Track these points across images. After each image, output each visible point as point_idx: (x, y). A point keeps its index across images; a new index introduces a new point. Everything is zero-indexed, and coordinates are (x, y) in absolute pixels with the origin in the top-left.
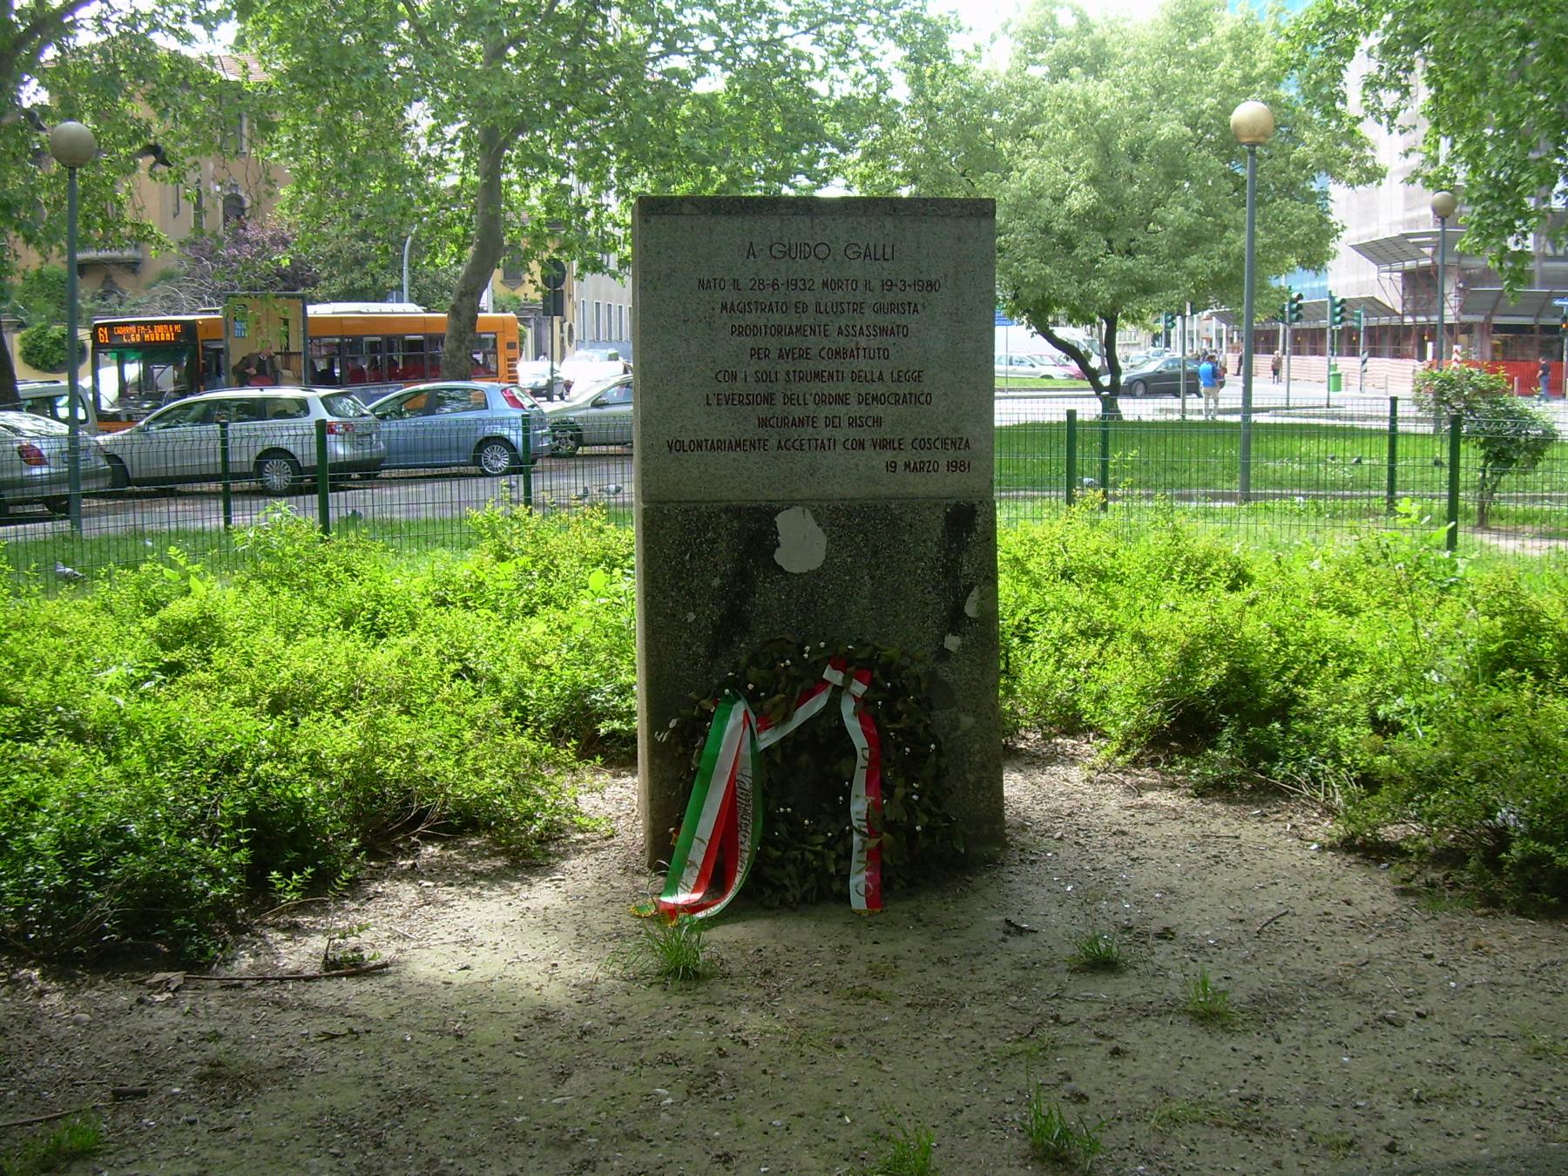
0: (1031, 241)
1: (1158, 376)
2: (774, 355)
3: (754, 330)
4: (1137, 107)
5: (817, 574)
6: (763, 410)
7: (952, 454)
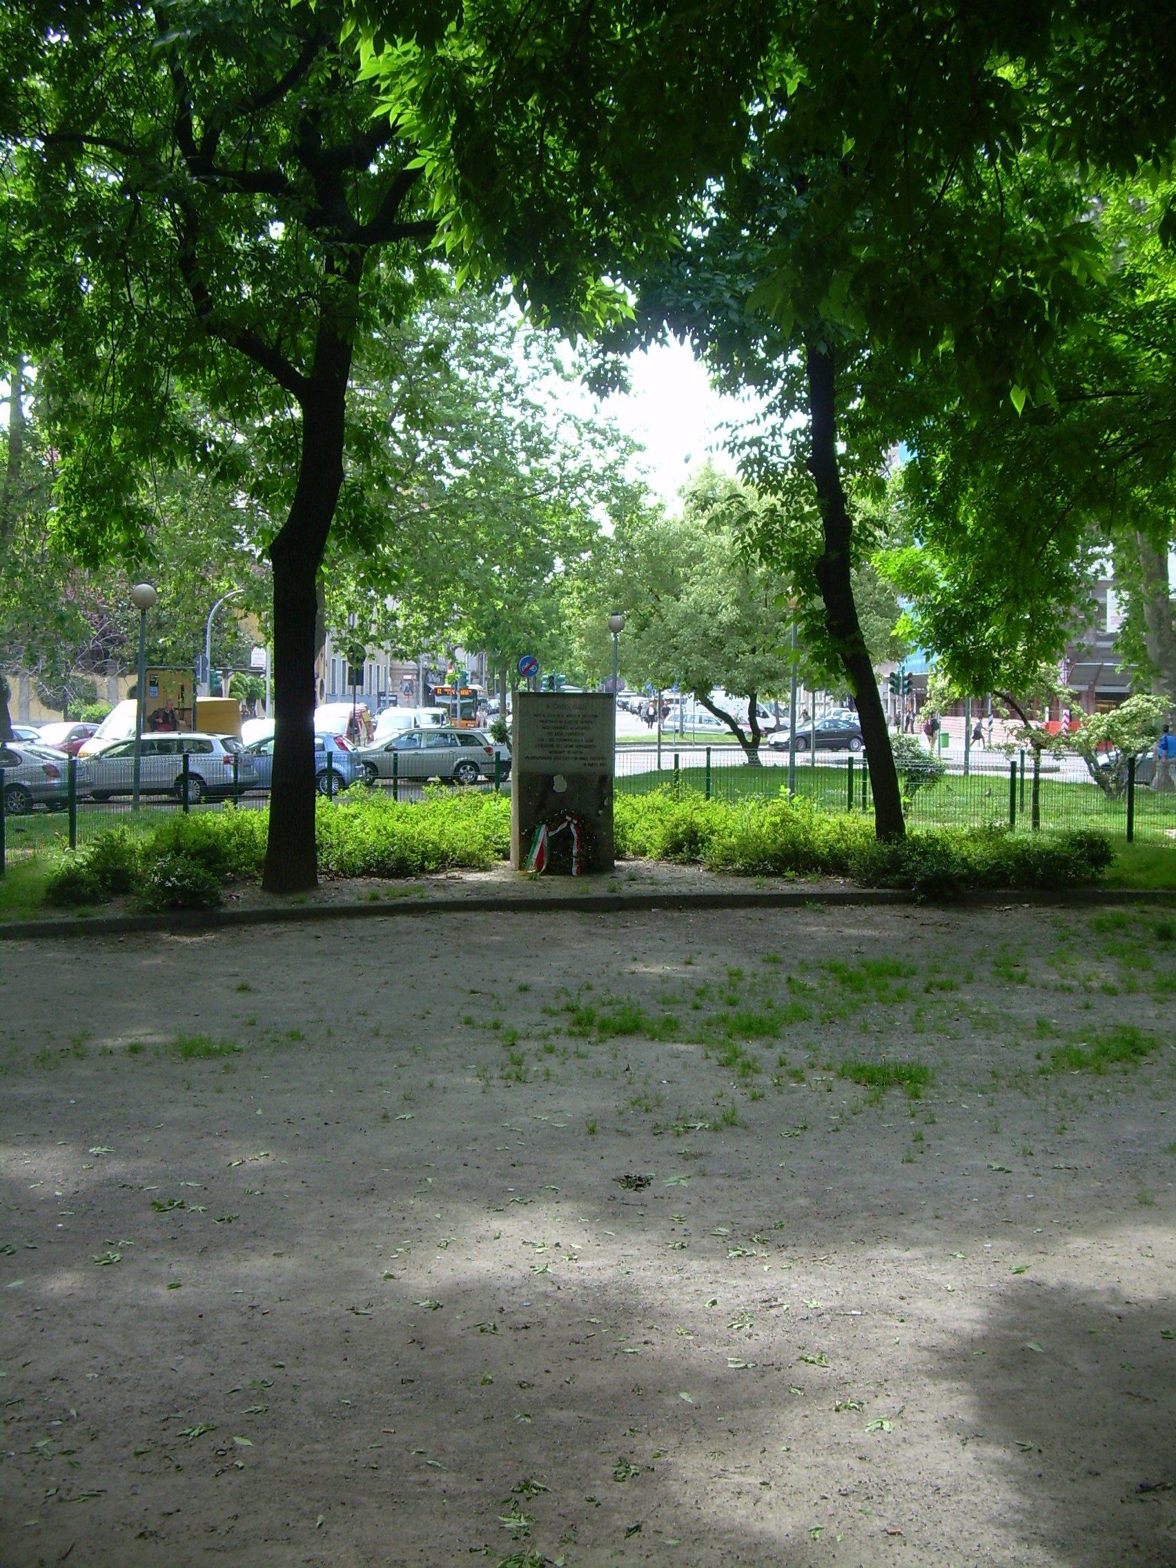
0: (694, 641)
3: (548, 728)
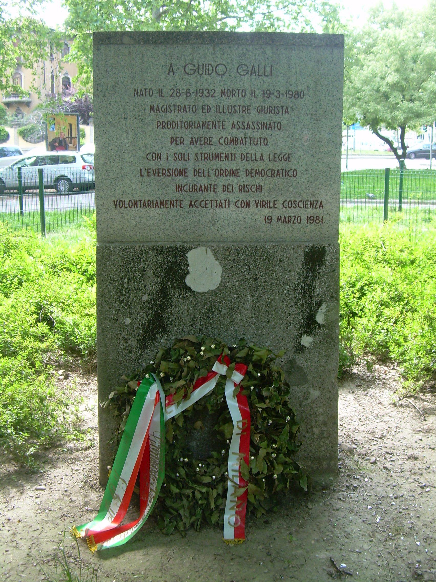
1: (421, 151)
2: (187, 142)
3: (173, 125)
4: (415, 41)
5: (215, 293)
6: (180, 180)
7: (310, 211)
